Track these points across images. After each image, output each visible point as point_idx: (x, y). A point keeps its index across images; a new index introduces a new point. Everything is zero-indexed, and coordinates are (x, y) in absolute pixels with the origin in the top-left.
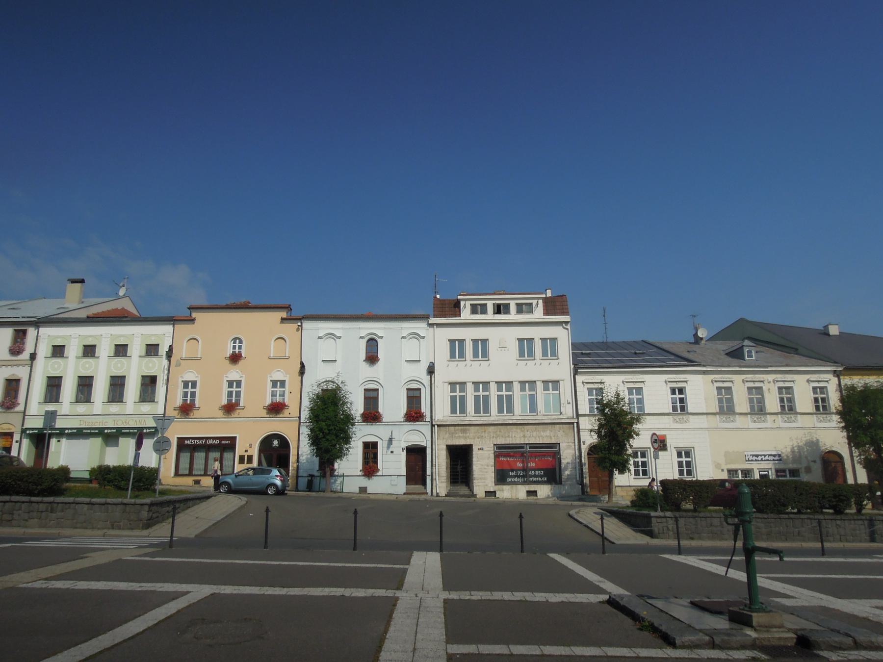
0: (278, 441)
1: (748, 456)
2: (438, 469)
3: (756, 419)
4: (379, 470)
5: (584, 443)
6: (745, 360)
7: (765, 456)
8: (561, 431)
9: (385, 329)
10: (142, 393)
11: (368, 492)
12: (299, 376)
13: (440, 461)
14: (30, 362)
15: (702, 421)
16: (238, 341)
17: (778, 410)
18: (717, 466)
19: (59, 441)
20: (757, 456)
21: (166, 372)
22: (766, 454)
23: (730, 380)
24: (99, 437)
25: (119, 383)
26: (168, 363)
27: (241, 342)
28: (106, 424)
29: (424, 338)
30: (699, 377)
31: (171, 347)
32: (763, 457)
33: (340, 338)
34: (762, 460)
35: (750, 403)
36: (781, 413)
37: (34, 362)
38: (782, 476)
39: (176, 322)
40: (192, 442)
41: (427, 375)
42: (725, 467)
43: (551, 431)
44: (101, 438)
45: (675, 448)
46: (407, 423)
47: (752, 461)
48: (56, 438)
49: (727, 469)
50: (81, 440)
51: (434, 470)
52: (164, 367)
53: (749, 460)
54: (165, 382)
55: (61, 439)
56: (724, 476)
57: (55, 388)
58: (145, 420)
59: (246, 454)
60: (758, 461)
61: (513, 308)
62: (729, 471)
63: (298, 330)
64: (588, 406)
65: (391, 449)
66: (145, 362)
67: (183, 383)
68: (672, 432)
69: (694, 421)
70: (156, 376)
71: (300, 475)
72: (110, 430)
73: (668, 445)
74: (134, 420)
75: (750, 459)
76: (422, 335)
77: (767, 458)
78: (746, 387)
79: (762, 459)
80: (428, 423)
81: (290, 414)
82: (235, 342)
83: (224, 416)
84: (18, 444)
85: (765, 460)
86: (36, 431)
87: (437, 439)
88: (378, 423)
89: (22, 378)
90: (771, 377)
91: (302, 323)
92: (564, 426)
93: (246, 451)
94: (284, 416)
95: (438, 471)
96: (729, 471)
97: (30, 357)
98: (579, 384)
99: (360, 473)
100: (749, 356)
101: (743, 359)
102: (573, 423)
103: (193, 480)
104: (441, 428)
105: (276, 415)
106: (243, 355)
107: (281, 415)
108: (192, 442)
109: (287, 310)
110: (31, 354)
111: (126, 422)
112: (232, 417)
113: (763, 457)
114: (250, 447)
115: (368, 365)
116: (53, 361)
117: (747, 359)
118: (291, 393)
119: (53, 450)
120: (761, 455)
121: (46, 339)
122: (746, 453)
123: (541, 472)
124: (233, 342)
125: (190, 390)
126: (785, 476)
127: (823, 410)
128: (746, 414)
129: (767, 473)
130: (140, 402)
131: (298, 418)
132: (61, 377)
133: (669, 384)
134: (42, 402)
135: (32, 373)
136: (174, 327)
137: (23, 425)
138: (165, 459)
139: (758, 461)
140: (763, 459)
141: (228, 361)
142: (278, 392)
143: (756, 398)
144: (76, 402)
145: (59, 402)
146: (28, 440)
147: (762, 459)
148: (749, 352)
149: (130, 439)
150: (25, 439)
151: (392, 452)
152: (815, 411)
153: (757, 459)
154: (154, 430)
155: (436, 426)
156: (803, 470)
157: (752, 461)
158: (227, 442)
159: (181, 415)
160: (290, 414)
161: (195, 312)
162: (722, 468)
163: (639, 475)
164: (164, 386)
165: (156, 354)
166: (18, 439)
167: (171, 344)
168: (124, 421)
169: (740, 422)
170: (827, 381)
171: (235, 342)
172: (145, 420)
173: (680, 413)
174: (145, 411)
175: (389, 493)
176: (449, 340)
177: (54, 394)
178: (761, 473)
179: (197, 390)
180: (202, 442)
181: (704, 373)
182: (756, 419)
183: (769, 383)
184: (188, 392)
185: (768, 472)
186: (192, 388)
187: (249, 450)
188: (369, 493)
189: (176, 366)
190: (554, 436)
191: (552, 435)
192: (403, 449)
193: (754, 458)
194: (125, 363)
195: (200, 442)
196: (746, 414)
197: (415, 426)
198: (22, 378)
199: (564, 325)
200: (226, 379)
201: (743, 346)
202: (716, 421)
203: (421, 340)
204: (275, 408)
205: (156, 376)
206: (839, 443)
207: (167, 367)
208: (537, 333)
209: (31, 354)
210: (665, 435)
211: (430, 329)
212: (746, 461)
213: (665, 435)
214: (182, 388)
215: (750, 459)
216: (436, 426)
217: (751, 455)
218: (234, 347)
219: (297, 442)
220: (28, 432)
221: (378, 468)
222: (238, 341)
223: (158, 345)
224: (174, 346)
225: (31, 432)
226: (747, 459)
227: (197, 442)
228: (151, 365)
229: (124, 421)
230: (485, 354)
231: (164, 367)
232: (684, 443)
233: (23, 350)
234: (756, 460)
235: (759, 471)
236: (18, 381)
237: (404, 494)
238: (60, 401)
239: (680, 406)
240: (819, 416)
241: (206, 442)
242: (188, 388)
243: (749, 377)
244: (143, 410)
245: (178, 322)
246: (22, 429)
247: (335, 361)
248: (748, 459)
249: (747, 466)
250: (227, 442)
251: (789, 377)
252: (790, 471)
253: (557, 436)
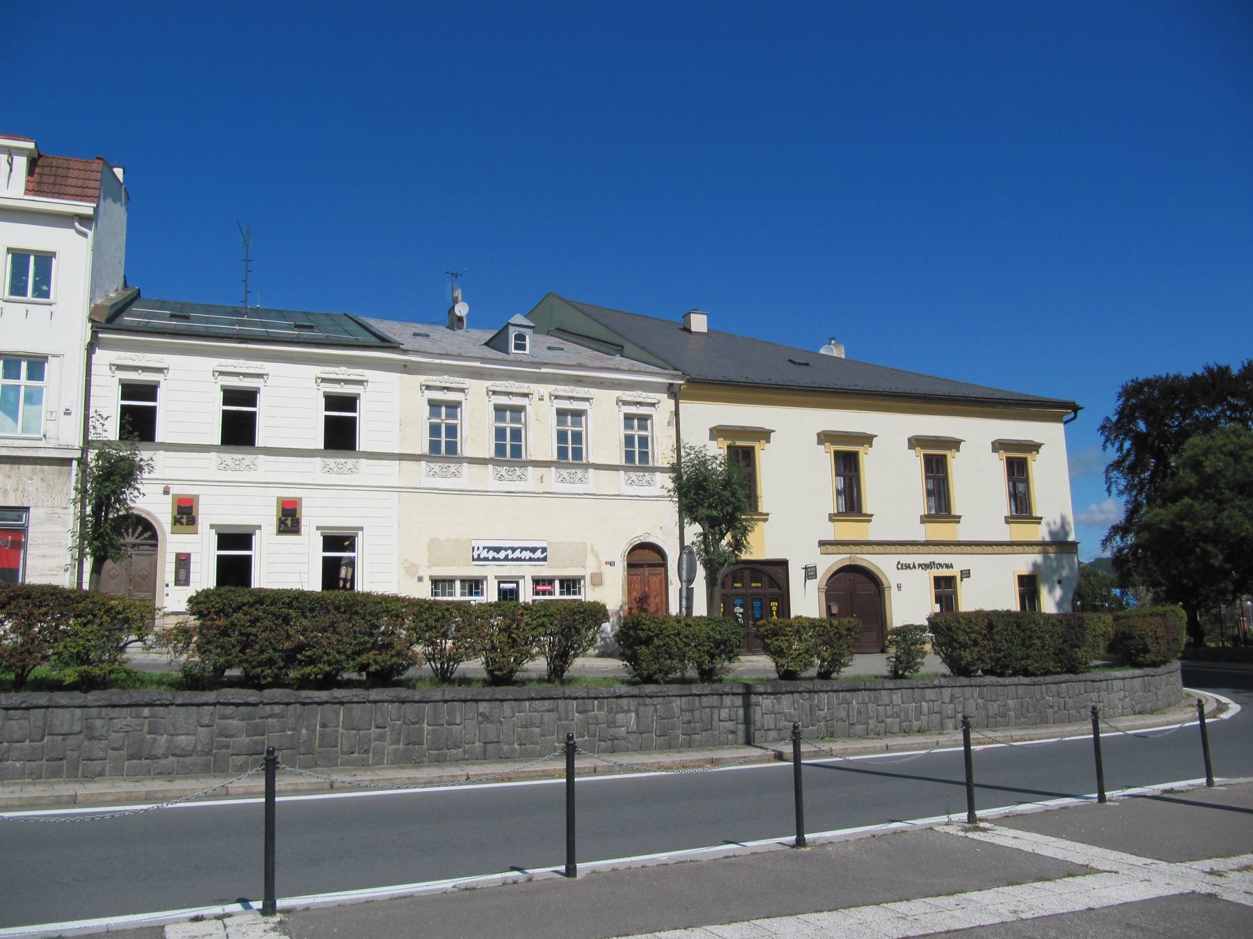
3: (634, 478)
6: (508, 353)
7: (514, 550)
8: (37, 480)
15: (390, 472)
18: (410, 568)
20: (497, 550)
32: (509, 552)
34: (506, 559)
35: (559, 442)
36: (625, 469)
38: (544, 593)
42: (427, 573)
43: (9, 477)
45: (318, 528)
47: (486, 559)
49: (532, 577)
53: (479, 559)
56: (423, 592)
60: (499, 560)
62: (436, 582)
64: (494, 442)
73: (304, 522)
75: (482, 557)
77: (517, 554)
79: (507, 556)
85: (513, 560)
90: (545, 389)
96: (436, 582)
100: (518, 347)
101: (507, 352)
102: (67, 462)
113: (509, 552)
117: (527, 351)
120: (506, 549)
122: (474, 544)
126: (551, 593)
127: (639, 462)
128: (483, 461)
129: (514, 585)
139: (499, 560)
143: (572, 431)
147: (507, 556)
148: (520, 337)
152: (623, 463)
153: (533, 556)
156: (588, 579)
157: (486, 559)
162: (420, 574)
169: (469, 476)
170: (653, 405)
173: (572, 464)
176: (9, 250)
178: (502, 585)
181: (406, 368)
183: (540, 399)
185: (517, 583)
190: (16, 490)
191: (8, 487)
193: (492, 554)
196: (483, 461)
199: (77, 224)
201: (509, 323)
202: (420, 473)
206: (661, 528)
210: (197, 496)
212: (474, 560)
213: (197, 496)
215: (482, 557)
217: (484, 548)
226: (476, 557)
230: (42, 291)
232: (339, 520)
234: (494, 559)
235: (499, 583)
239: (446, 441)
240: (631, 474)
243: (501, 385)
248: (479, 555)
249: (474, 571)
251: (581, 391)
252: (562, 582)
253: (24, 489)
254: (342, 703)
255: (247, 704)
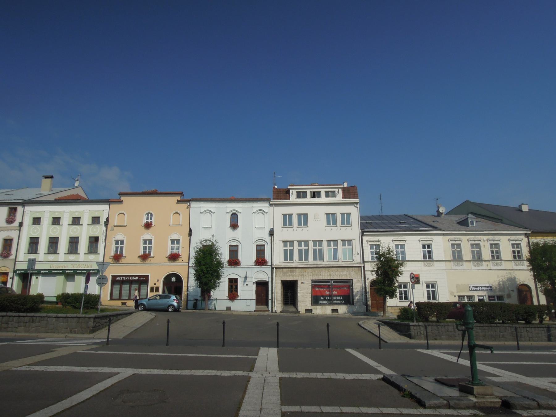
0: (175, 278)
1: (471, 287)
2: (276, 295)
3: (476, 264)
4: (239, 296)
5: (368, 279)
6: (469, 227)
7: (482, 287)
8: (353, 272)
9: (242, 207)
10: (89, 248)
11: (232, 310)
12: (188, 237)
13: (277, 290)
14: (19, 228)
15: (442, 266)
16: (150, 215)
17: (490, 258)
18: (452, 293)
19: (37, 278)
20: (477, 287)
21: (105, 234)
22: (482, 286)
23: (460, 239)
24: (62, 275)
25: (75, 241)
26: (106, 228)
27: (152, 215)
28: (67, 267)
29: (267, 213)
30: (440, 238)
31: (107, 219)
32: (480, 288)
33: (214, 213)
34: (480, 290)
35: (472, 254)
36: (492, 260)
37: (21, 228)
38: (492, 300)
39: (111, 203)
40: (121, 279)
41: (269, 236)
42: (457, 294)
43: (347, 272)
44: (63, 276)
45: (425, 282)
46: (256, 266)
47: (474, 290)
48: (35, 276)
49: (458, 295)
50: (51, 277)
51: (273, 296)
52: (104, 231)
53: (471, 290)
54: (104, 240)
55: (38, 277)
56: (456, 300)
57: (35, 245)
58: (91, 265)
59: (155, 286)
60: (477, 290)
61: (323, 194)
62: (459, 297)
63: (187, 208)
64: (370, 256)
65: (246, 283)
66: (91, 228)
67: (115, 241)
68: (423, 272)
69: (437, 265)
70: (98, 237)
71: (189, 299)
72: (70, 271)
73: (421, 281)
74: (85, 265)
75: (472, 289)
76: (266, 211)
77: (483, 288)
78: (470, 244)
79: (480, 289)
80: (270, 266)
81: (182, 261)
82: (148, 216)
83: (141, 262)
84: (11, 280)
85: (482, 290)
86: (23, 272)
87: (275, 276)
88: (238, 267)
89: (14, 238)
90: (485, 238)
91: (190, 204)
92: (355, 268)
93: (155, 284)
94: (179, 262)
95: (276, 297)
96: (459, 297)
97: (19, 225)
98: (364, 242)
99: (227, 298)
100: (471, 224)
101: (468, 226)
103: (122, 302)
104: (278, 269)
105: (174, 261)
106: (153, 224)
107: (177, 262)
108: (121, 279)
109: (180, 195)
110: (19, 223)
111: (79, 266)
112: (146, 262)
113: (480, 288)
114: (158, 282)
115: (232, 230)
116: (34, 227)
117: (470, 226)
118: (183, 247)
119: (33, 284)
120: (479, 287)
121: (29, 214)
122: (470, 285)
123: (341, 298)
124: (146, 215)
125: (119, 246)
126: (494, 300)
127: (518, 258)
128: (470, 261)
129: (483, 298)
130: (88, 253)
131: (187, 263)
132: (38, 238)
133: (421, 242)
134: (26, 253)
135: (20, 235)
136: (109, 206)
137: (14, 268)
138: (104, 289)
139: (477, 290)
140: (481, 289)
141: (143, 227)
142: (175, 247)
143: (476, 250)
144: (48, 253)
145: (37, 253)
146: (18, 277)
147: (480, 289)
149: (82, 276)
150: (16, 277)
151: (247, 285)
152: (513, 259)
153: (477, 289)
154: (97, 271)
155: (275, 268)
156: (506, 296)
157: (474, 290)
158: (143, 279)
159: (114, 262)
160: (182, 261)
161: (123, 197)
162: (455, 295)
163: (402, 299)
164: (103, 243)
165: (98, 223)
166: (12, 277)
167: (108, 217)
168: (78, 265)
169: (466, 266)
170: (521, 240)
171: (148, 216)
172: (91, 265)
173: (428, 260)
174: (91, 259)
175: (245, 310)
176: (282, 214)
177: (34, 248)
178: (479, 298)
179: (124, 246)
180: (127, 278)
181: (443, 235)
182: (476, 264)
183: (484, 241)
184: (118, 247)
185: (484, 297)
186: (121, 244)
187: (157, 283)
188: (232, 311)
189: (111, 231)
190: (349, 275)
191: (347, 274)
192: (254, 283)
193: (475, 289)
194: (79, 229)
195: (126, 278)
196: (470, 261)
197: (262, 268)
198: (14, 238)
199: (355, 205)
200: (142, 239)
201: (468, 218)
202: (451, 265)
203: (265, 214)
204: (173, 257)
205: (98, 237)
206: (528, 279)
207: (105, 231)
208: (338, 210)
209: (19, 223)
210: (419, 274)
211: (271, 207)
212: (470, 290)
213: (419, 274)
214: (115, 244)
215: (472, 289)
216: (275, 268)
217: (473, 287)
218: (147, 219)
219: (187, 278)
220: (17, 272)
221: (238, 295)
222: (150, 215)
223: (99, 217)
224: (109, 218)
225: (20, 272)
226: (470, 289)
227: (124, 279)
228: (95, 230)
229: (78, 265)
230: (305, 223)
231: (104, 231)
232: (431, 279)
233: (15, 221)
234: (476, 290)
235: (478, 297)
236: (11, 240)
237: (255, 311)
238: (38, 253)
239: (428, 256)
240: (516, 262)
241: (129, 278)
242: (118, 244)
243: (472, 237)
244: (90, 259)
245: (112, 203)
246: (14, 270)
247: (211, 227)
248: (471, 289)
249: (470, 294)
250: (143, 279)
251: (497, 237)
252: (497, 296)
254: (499, 327)
255: (481, 326)
